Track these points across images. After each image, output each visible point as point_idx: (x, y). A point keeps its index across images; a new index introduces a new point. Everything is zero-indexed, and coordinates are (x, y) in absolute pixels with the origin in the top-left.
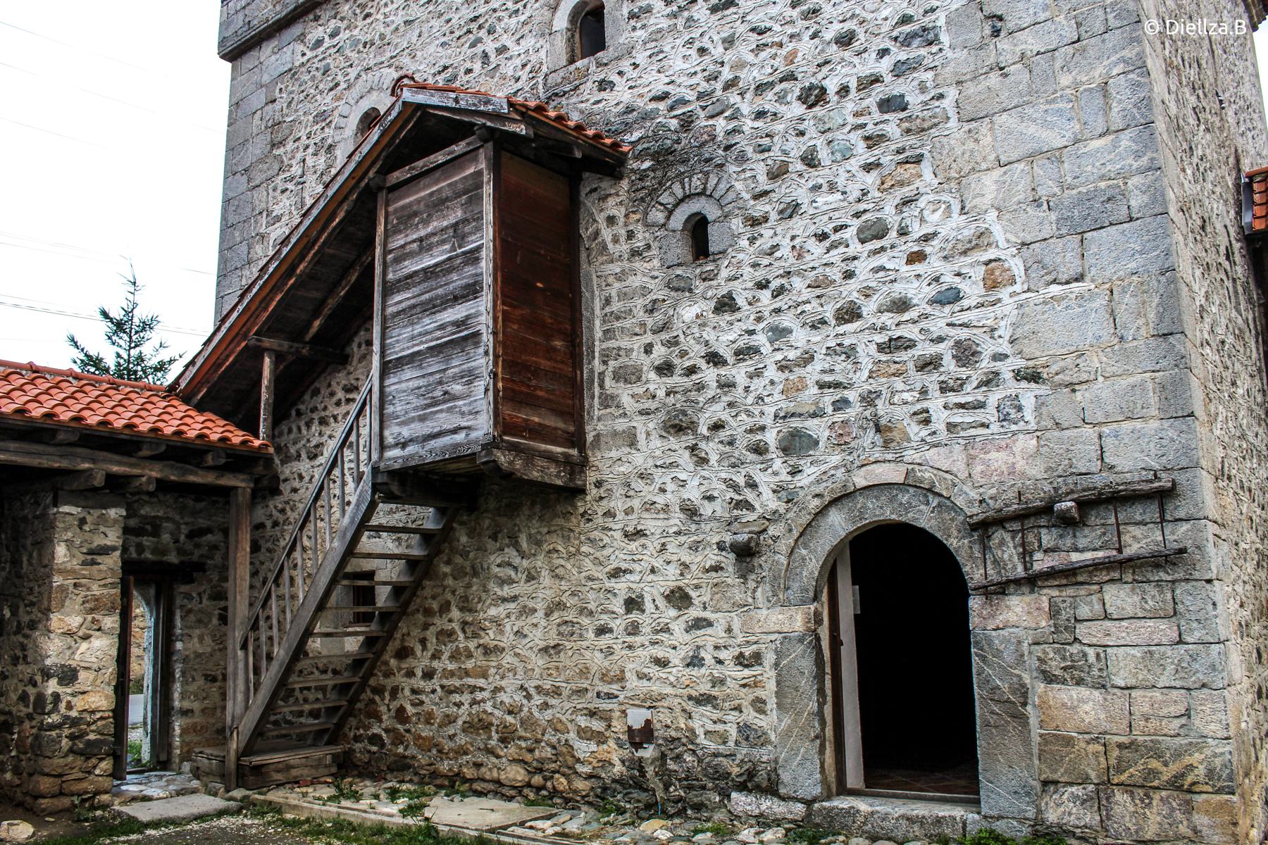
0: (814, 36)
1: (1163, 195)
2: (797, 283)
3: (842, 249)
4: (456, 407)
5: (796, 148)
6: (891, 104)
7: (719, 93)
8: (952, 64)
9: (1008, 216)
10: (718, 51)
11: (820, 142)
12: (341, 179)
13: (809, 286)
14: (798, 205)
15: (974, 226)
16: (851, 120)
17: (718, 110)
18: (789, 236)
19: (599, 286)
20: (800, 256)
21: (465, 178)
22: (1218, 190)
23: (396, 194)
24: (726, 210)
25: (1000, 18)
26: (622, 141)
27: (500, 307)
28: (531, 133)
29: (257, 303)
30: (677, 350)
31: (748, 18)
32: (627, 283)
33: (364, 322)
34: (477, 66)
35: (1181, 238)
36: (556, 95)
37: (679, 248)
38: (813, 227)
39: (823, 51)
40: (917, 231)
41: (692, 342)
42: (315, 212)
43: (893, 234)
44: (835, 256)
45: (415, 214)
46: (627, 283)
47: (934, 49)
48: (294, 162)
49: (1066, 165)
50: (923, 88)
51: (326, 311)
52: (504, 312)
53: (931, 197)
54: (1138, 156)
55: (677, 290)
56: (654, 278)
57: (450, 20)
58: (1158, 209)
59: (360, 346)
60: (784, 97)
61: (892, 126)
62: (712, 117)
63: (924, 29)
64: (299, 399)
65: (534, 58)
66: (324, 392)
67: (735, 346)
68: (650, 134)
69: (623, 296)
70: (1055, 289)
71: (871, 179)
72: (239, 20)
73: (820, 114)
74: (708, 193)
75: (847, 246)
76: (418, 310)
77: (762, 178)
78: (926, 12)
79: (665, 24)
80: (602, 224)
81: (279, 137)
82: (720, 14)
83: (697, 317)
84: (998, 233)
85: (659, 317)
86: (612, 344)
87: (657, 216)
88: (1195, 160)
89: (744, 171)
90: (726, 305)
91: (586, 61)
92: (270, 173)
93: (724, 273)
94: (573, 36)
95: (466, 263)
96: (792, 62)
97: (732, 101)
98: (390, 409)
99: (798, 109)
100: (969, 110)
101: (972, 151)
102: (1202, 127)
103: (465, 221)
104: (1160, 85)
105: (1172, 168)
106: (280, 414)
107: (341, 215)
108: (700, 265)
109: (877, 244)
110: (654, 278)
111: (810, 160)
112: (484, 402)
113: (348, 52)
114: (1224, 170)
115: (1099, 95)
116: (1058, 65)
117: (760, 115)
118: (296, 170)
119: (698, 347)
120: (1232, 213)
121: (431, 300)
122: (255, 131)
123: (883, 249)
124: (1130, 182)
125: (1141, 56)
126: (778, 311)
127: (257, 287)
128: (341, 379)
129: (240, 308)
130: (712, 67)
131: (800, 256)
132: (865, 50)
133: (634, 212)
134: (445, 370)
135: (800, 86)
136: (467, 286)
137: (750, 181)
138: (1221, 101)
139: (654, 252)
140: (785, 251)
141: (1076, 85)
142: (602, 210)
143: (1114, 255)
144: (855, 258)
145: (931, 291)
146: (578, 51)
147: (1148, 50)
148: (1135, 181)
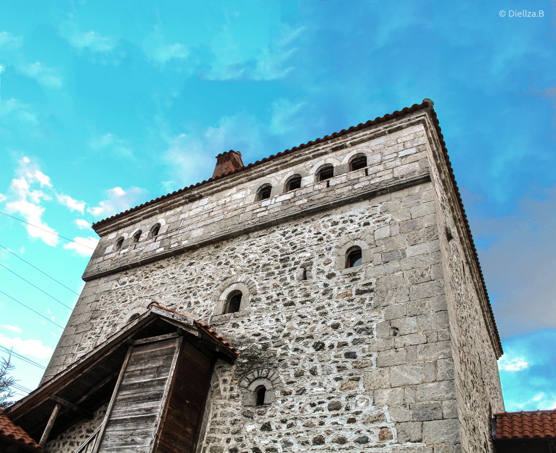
0: (323, 323)
1: (456, 410)
2: (299, 423)
3: (320, 412)
4: (135, 447)
5: (308, 366)
6: (349, 355)
7: (281, 338)
8: (377, 343)
9: (392, 409)
10: (284, 321)
11: (319, 365)
12: (115, 337)
13: (304, 426)
14: (305, 390)
15: (378, 411)
16: (333, 358)
17: (279, 344)
18: (299, 402)
19: (213, 408)
20: (302, 412)
21: (168, 349)
22: (481, 416)
23: (137, 348)
24: (274, 386)
25: (397, 329)
26: (237, 349)
27: (167, 407)
28: (200, 336)
29: (61, 380)
30: (241, 443)
31: (298, 311)
32: (225, 410)
33: (106, 402)
34: (185, 307)
35: (464, 431)
36: (214, 325)
37: (251, 399)
38: (310, 400)
39: (326, 329)
40: (354, 409)
41: (248, 441)
42: (100, 348)
43: (343, 409)
44: (317, 414)
45: (143, 359)
46: (225, 410)
47: (370, 336)
48: (98, 327)
49: (418, 392)
50: (364, 351)
51: (91, 393)
52: (169, 410)
53: (361, 396)
54: (447, 392)
55: (246, 416)
56: (238, 409)
57: (179, 287)
58: (454, 416)
59: (100, 412)
60: (307, 344)
61: (349, 364)
62: (276, 347)
63: (367, 328)
64: (64, 431)
65: (209, 309)
66: (77, 430)
67: (267, 446)
68: (249, 349)
69: (222, 415)
70: (409, 444)
71: (337, 384)
72: (95, 267)
73: (320, 354)
74: (268, 378)
75: (323, 411)
76: (132, 400)
77: (292, 376)
78: (369, 322)
79: (265, 306)
80: (221, 382)
81: (96, 316)
82: (287, 307)
83: (253, 430)
84: (387, 415)
85: (236, 427)
86: (213, 435)
87: (245, 383)
88: (471, 401)
89: (285, 371)
90: (266, 427)
91: (230, 314)
92: (86, 329)
93: (268, 413)
94: (227, 304)
95: (158, 385)
96: (313, 331)
97: (286, 342)
98: (105, 442)
99: (312, 350)
100: (381, 363)
101: (380, 380)
102: (475, 389)
103: (163, 366)
104: (457, 367)
105: (461, 401)
106: (54, 434)
107: (111, 352)
108: (259, 408)
109: (335, 412)
110: (238, 409)
111: (313, 372)
112: (149, 448)
113: (135, 289)
114: (484, 410)
115: (433, 366)
116: (418, 351)
117: (296, 350)
118: (98, 331)
119: (250, 444)
120: (487, 428)
121: (138, 397)
122: (86, 311)
123: (338, 415)
124: (443, 403)
125: (450, 353)
126: (288, 434)
127: (64, 374)
128: (87, 425)
129: (53, 381)
130: (280, 327)
131: (302, 412)
132: (343, 332)
133: (235, 380)
134: (135, 430)
135: (314, 341)
136: (156, 394)
137: (287, 376)
138: (483, 382)
139: (240, 398)
140: (296, 409)
141: (425, 360)
142: (222, 376)
143: (435, 433)
144: (325, 417)
145: (356, 437)
146: (227, 310)
147: (453, 351)
148: (445, 403)
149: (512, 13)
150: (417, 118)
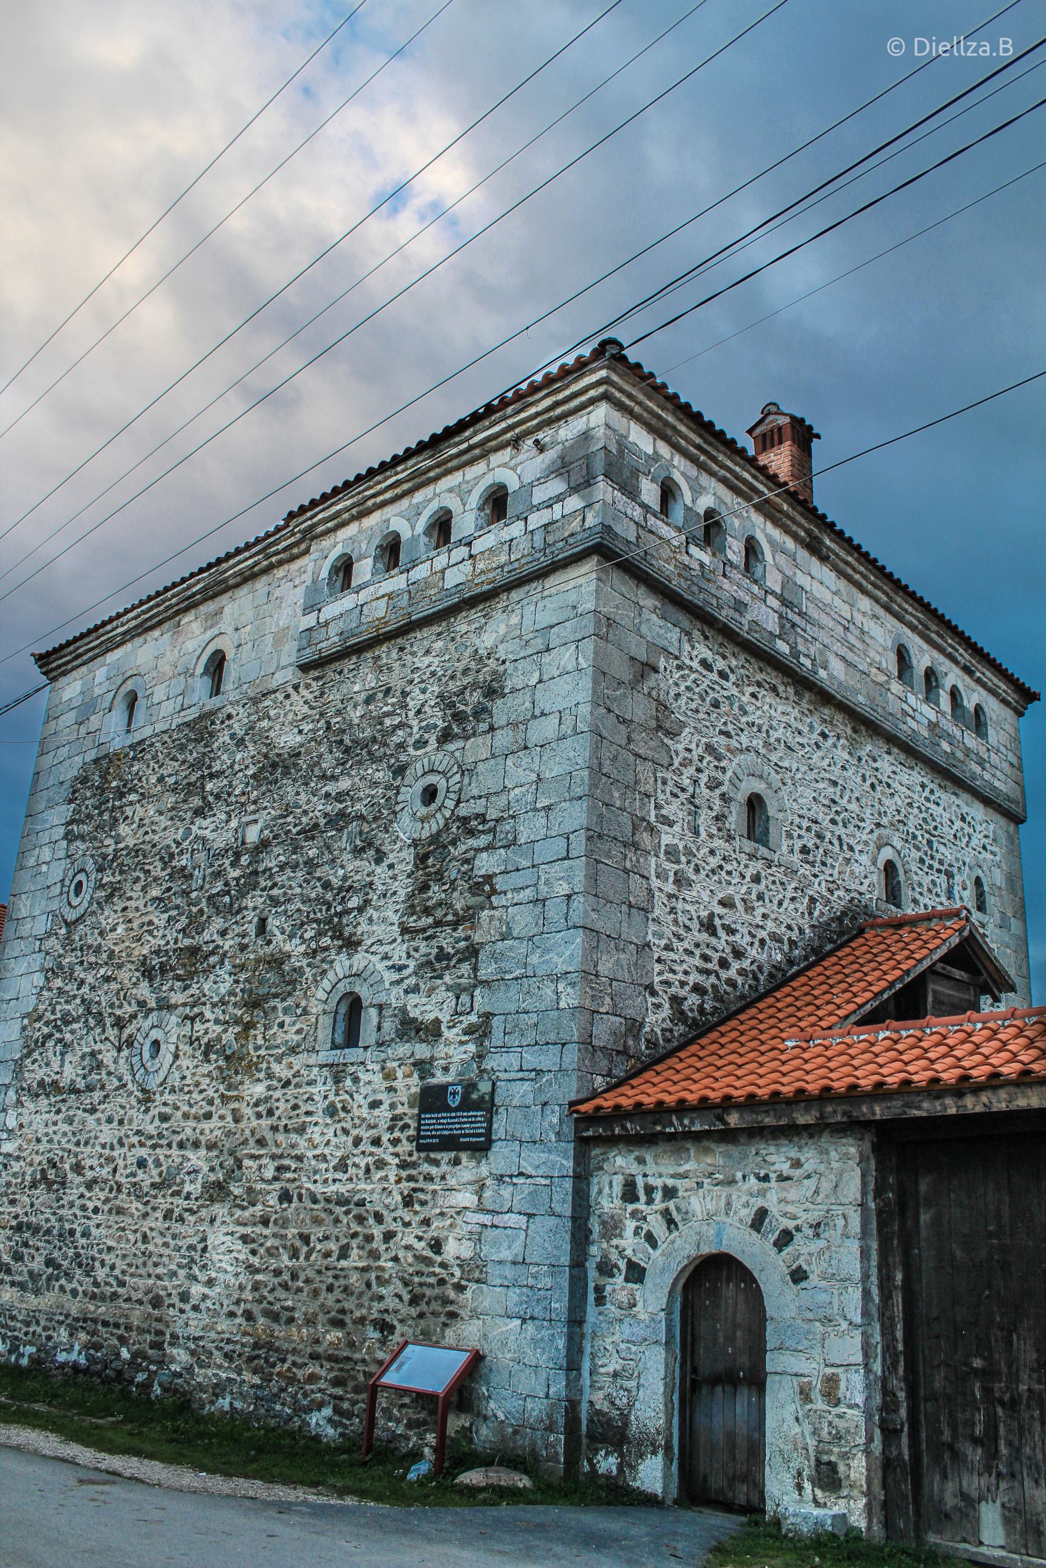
149: (922, 47)
150: (630, 396)
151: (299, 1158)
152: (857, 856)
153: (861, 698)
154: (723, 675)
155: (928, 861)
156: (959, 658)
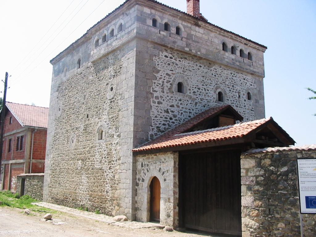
151: (94, 161)
152: (210, 92)
153: (210, 57)
154: (171, 58)
155: (232, 90)
156: (243, 42)
